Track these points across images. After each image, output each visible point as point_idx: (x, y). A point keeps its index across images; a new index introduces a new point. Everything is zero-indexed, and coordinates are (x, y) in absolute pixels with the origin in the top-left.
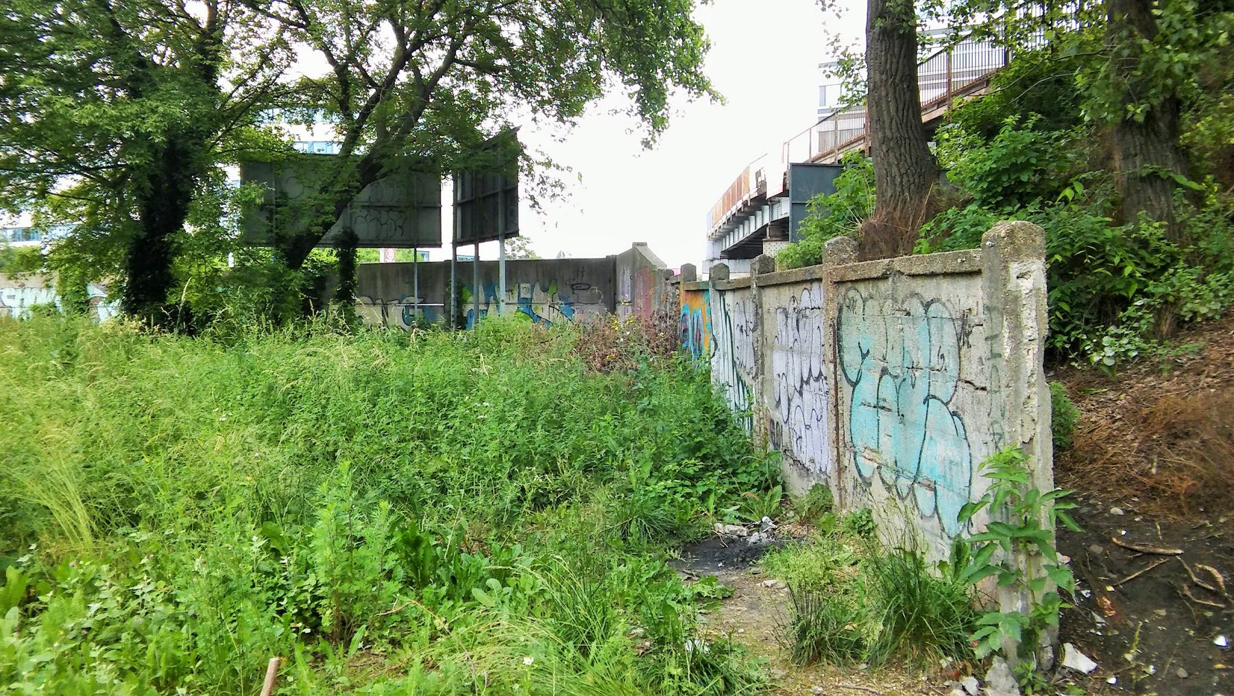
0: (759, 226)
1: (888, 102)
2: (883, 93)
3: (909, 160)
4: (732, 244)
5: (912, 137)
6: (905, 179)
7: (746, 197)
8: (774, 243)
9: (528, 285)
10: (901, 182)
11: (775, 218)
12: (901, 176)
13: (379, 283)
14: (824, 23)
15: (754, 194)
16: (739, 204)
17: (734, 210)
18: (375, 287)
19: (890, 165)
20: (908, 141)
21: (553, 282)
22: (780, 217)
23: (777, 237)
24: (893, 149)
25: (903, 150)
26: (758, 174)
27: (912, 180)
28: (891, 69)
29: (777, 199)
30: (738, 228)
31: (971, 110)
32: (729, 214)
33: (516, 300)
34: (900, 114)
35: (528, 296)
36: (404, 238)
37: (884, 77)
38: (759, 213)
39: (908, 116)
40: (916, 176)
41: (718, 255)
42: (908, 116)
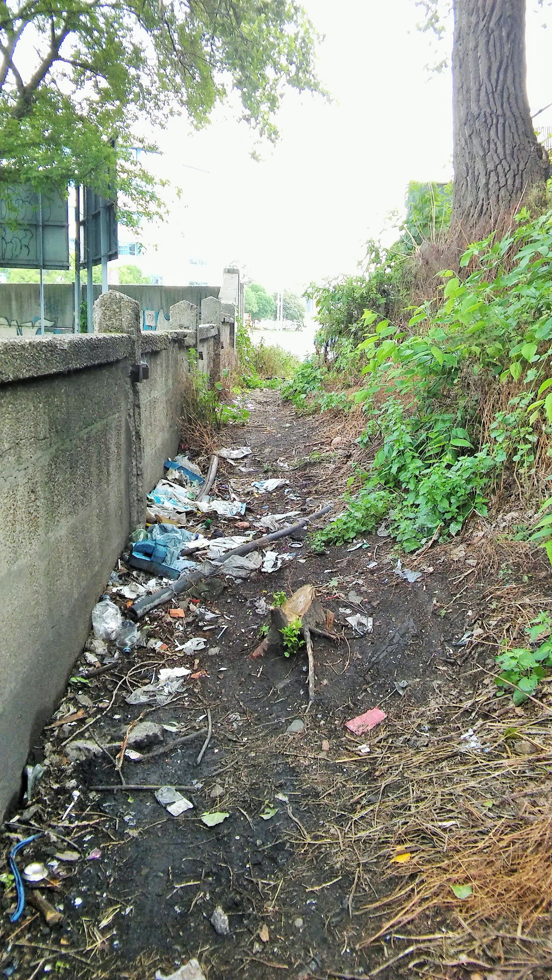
1: (477, 59)
2: (471, 45)
3: (500, 150)
5: (508, 114)
6: (493, 179)
9: (153, 313)
10: (487, 184)
12: (488, 175)
13: (14, 303)
18: (10, 308)
19: (473, 158)
20: (501, 120)
24: (479, 133)
25: (493, 132)
27: (502, 181)
28: (484, 6)
31: (397, 963)
34: (494, 76)
36: (30, 257)
37: (473, 19)
39: (505, 81)
40: (510, 175)
42: (505, 81)
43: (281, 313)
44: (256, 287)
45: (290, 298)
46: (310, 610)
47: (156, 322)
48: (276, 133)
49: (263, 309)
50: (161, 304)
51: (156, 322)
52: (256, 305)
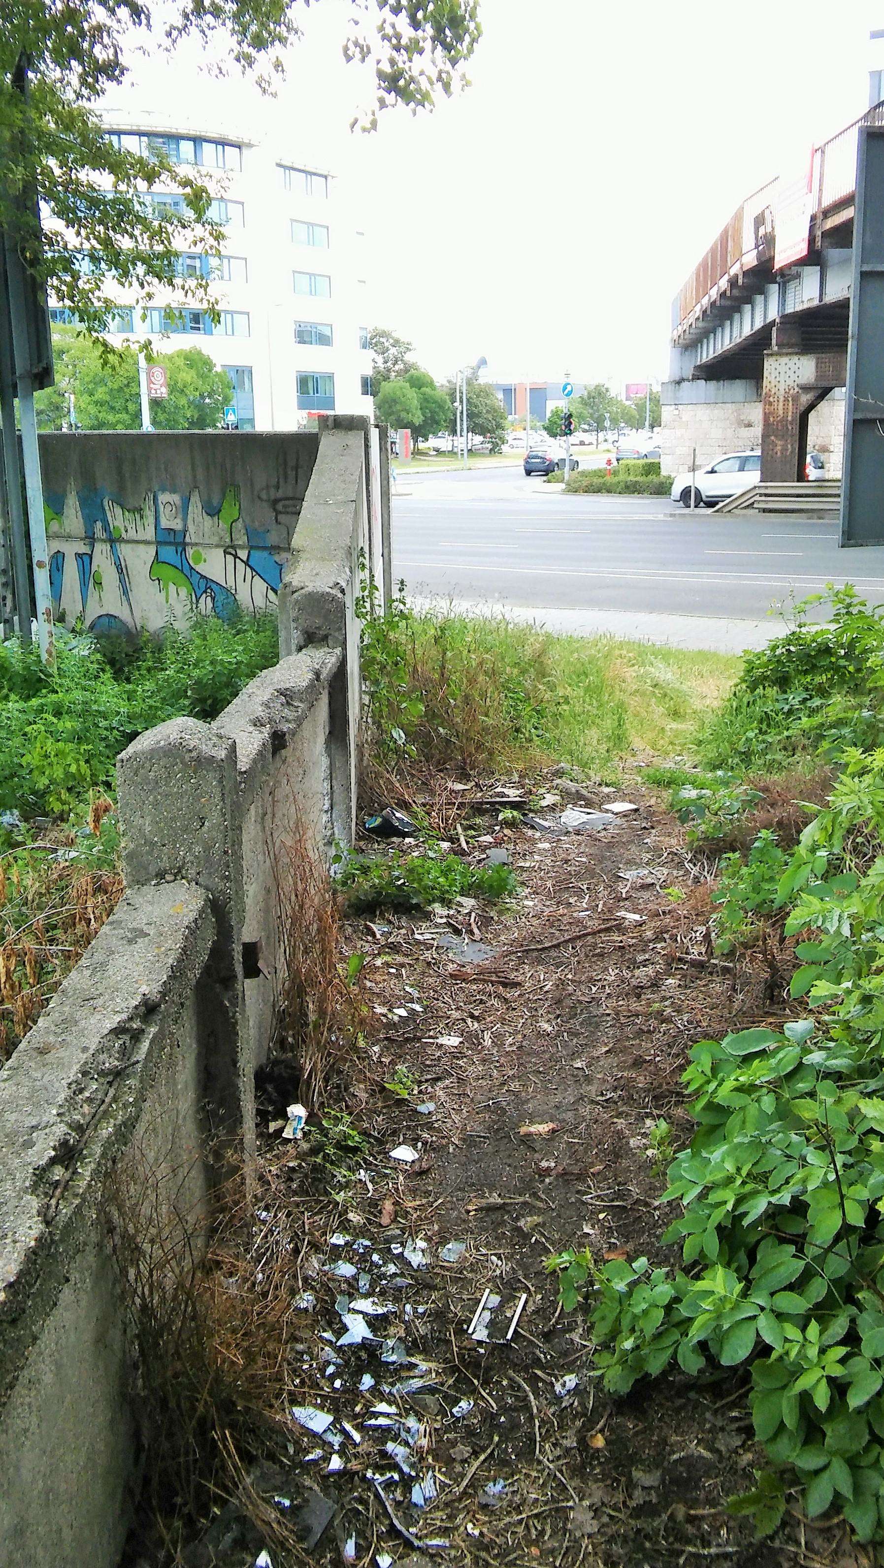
0: (759, 324)
4: (711, 356)
7: (735, 270)
8: (784, 360)
9: (175, 498)
11: (789, 310)
14: (160, 46)
15: (750, 260)
16: (723, 283)
17: (714, 293)
21: (230, 496)
22: (799, 308)
23: (791, 346)
26: (759, 221)
29: (794, 269)
30: (722, 326)
32: (705, 301)
33: (149, 533)
35: (177, 525)
38: (759, 299)
41: (689, 373)
43: (463, 424)
44: (418, 379)
45: (478, 396)
46: (212, 1214)
47: (185, 520)
48: (456, 22)
49: (432, 418)
50: (195, 477)
51: (185, 520)
52: (419, 412)
